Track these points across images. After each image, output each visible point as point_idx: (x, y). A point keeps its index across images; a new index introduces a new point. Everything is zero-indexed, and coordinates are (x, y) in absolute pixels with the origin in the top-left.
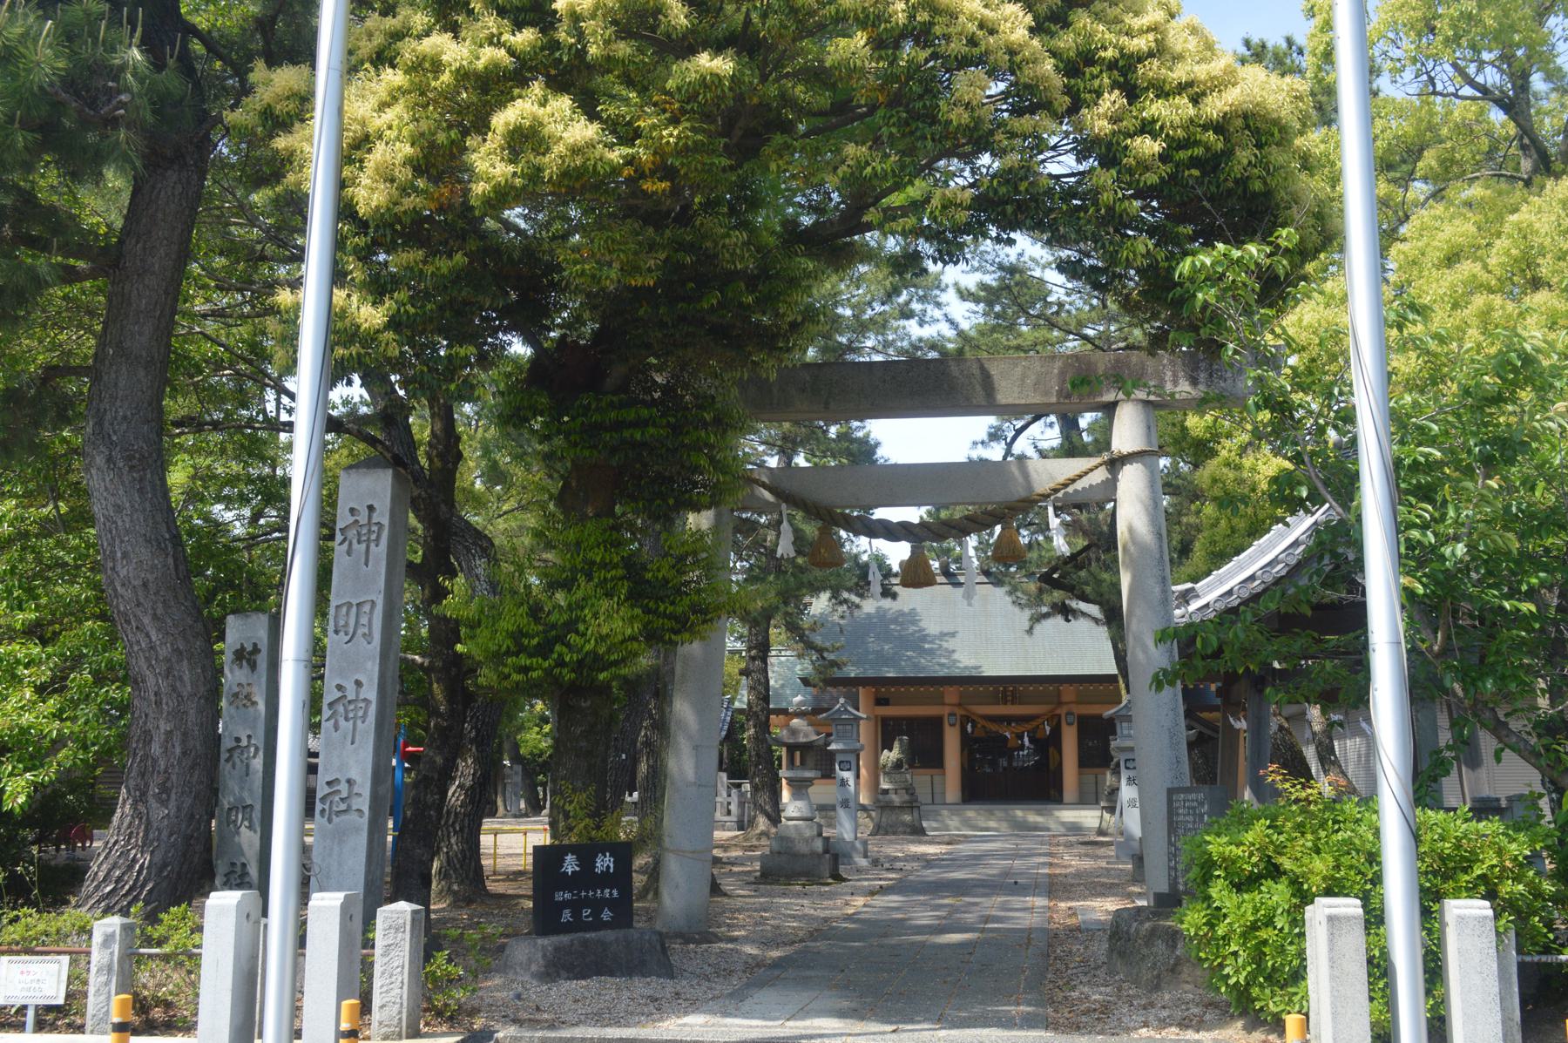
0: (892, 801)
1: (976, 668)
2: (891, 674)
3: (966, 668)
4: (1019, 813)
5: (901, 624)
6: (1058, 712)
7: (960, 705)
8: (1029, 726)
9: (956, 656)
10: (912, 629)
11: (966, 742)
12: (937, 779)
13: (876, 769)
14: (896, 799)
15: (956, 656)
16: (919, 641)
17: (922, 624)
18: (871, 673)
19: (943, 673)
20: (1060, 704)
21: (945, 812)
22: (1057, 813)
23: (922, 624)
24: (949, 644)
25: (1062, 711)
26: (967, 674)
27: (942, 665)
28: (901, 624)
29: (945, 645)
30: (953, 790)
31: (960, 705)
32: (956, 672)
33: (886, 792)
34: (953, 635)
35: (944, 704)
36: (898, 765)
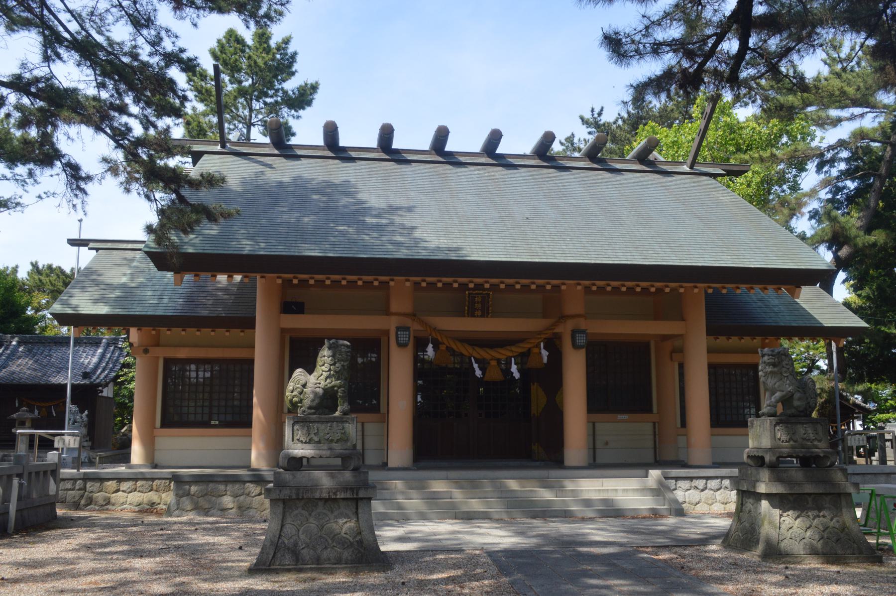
0: (315, 487)
1: (458, 249)
2: (313, 251)
3: (438, 249)
4: (513, 485)
5: (328, 194)
6: (558, 330)
7: (413, 316)
8: (517, 349)
9: (417, 234)
10: (345, 201)
11: (423, 373)
12: (371, 428)
13: (283, 410)
14: (324, 480)
15: (417, 234)
16: (357, 215)
17: (360, 196)
18: (281, 250)
19: (402, 254)
20: (563, 318)
21: (399, 484)
22: (570, 485)
23: (360, 196)
24: (407, 220)
25: (565, 330)
26: (441, 256)
27: (398, 244)
28: (328, 194)
29: (398, 220)
30: (400, 449)
31: (413, 316)
32: (423, 254)
33: (296, 463)
34: (410, 209)
35: (387, 312)
36: (326, 401)
